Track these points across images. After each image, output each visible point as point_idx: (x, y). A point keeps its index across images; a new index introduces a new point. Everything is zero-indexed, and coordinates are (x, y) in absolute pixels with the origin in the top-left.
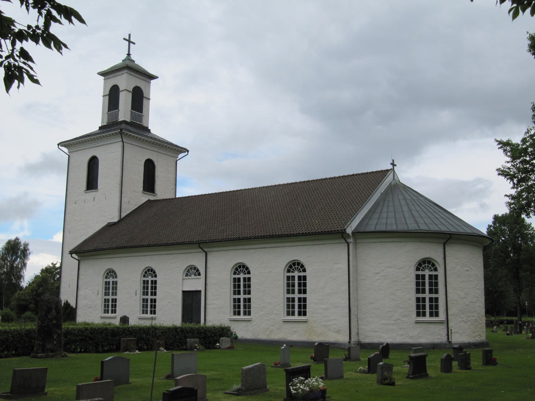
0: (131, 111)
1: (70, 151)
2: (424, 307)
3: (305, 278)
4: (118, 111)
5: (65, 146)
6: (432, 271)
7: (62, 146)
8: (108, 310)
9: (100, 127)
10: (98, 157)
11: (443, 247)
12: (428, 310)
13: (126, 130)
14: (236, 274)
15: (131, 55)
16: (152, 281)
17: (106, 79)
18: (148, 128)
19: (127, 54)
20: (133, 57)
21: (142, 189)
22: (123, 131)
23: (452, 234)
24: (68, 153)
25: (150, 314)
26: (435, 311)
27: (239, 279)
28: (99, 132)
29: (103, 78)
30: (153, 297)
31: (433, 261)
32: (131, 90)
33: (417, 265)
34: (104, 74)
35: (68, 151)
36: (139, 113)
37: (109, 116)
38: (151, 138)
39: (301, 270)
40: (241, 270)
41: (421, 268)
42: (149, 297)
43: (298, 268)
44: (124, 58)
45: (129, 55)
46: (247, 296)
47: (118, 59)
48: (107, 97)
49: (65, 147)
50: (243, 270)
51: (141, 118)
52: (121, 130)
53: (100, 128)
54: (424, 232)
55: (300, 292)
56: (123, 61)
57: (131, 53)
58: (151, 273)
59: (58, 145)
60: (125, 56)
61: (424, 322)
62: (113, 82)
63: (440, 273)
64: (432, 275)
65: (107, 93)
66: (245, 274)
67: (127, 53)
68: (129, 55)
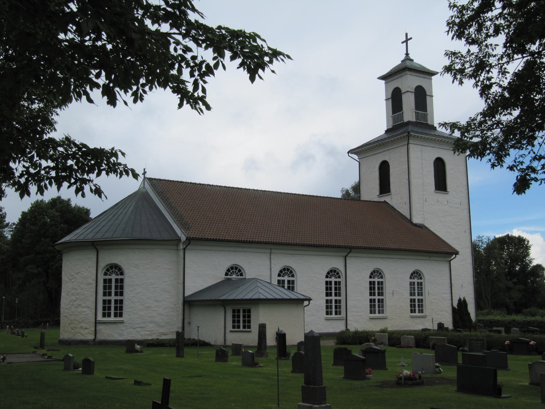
0: (416, 112)
1: (360, 157)
2: (109, 308)
3: (122, 281)
4: (403, 113)
5: (355, 153)
6: (290, 277)
7: (352, 153)
8: (415, 310)
9: (386, 131)
10: (389, 161)
11: (96, 254)
12: (113, 312)
13: (413, 131)
14: (280, 276)
15: (409, 54)
16: (418, 283)
17: (388, 82)
18: (434, 125)
19: (405, 54)
20: (411, 56)
21: (434, 188)
22: (411, 133)
23: (95, 241)
24: (358, 160)
25: (418, 313)
26: (247, 315)
27: (110, 280)
28: (386, 136)
29: (383, 82)
30: (373, 297)
31: (294, 273)
32: (413, 91)
33: (282, 269)
34: (383, 78)
35: (358, 158)
36: (424, 113)
37: (394, 119)
38: (439, 136)
39: (119, 273)
40: (233, 272)
41: (284, 272)
42: (416, 297)
43: (115, 271)
44: (402, 59)
45: (407, 54)
46: (329, 298)
47: (396, 61)
48: (390, 101)
49: (354, 154)
50: (115, 271)
51: (425, 117)
52: (409, 133)
53: (387, 132)
54: (130, 240)
55: (116, 294)
56: (402, 61)
57: (409, 53)
58: (285, 273)
59: (348, 153)
60: (403, 57)
61: (109, 323)
62: (396, 83)
63: (342, 279)
64: (118, 279)
65: (390, 96)
66: (118, 275)
67: (405, 53)
68: (407, 54)
